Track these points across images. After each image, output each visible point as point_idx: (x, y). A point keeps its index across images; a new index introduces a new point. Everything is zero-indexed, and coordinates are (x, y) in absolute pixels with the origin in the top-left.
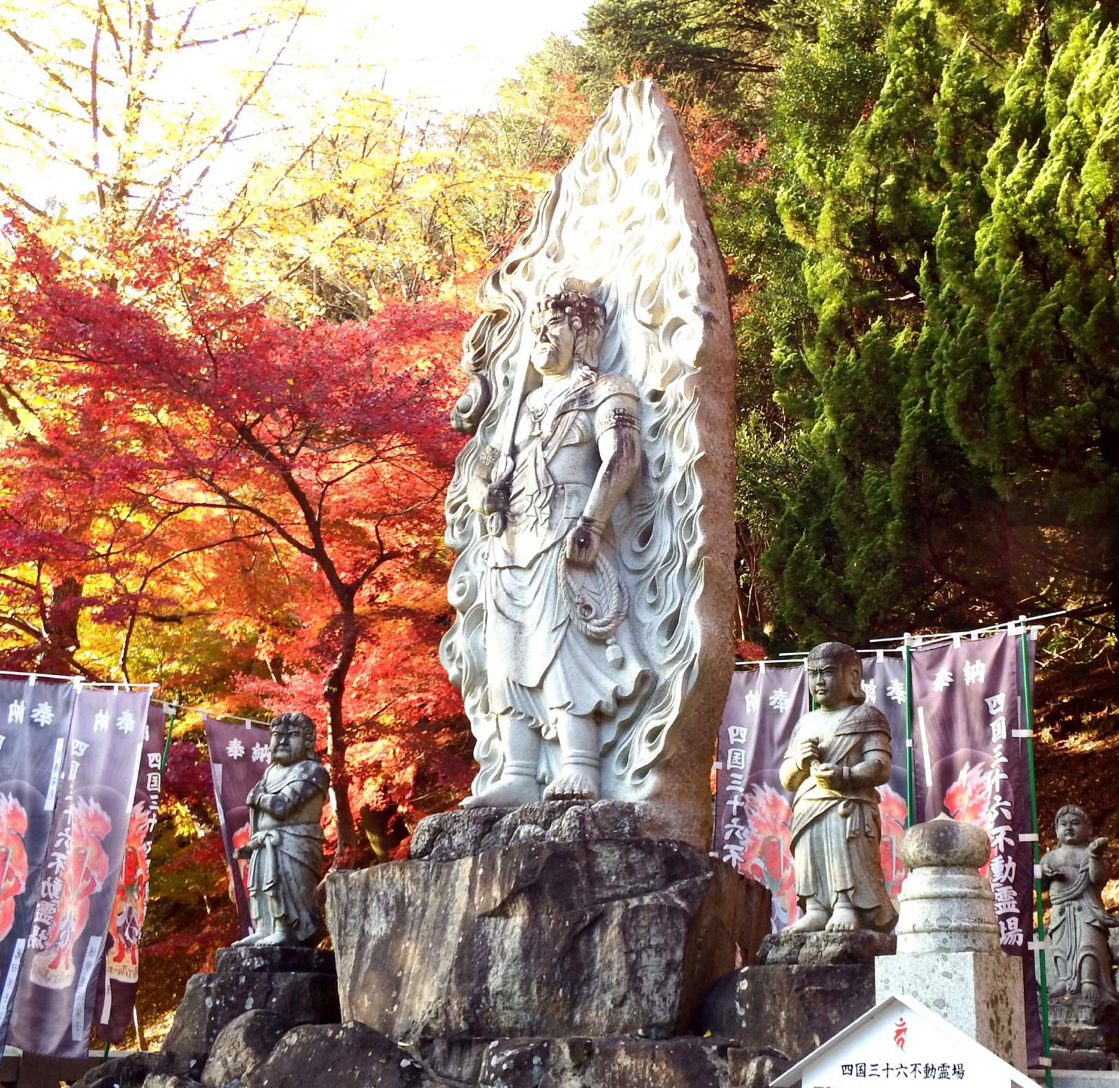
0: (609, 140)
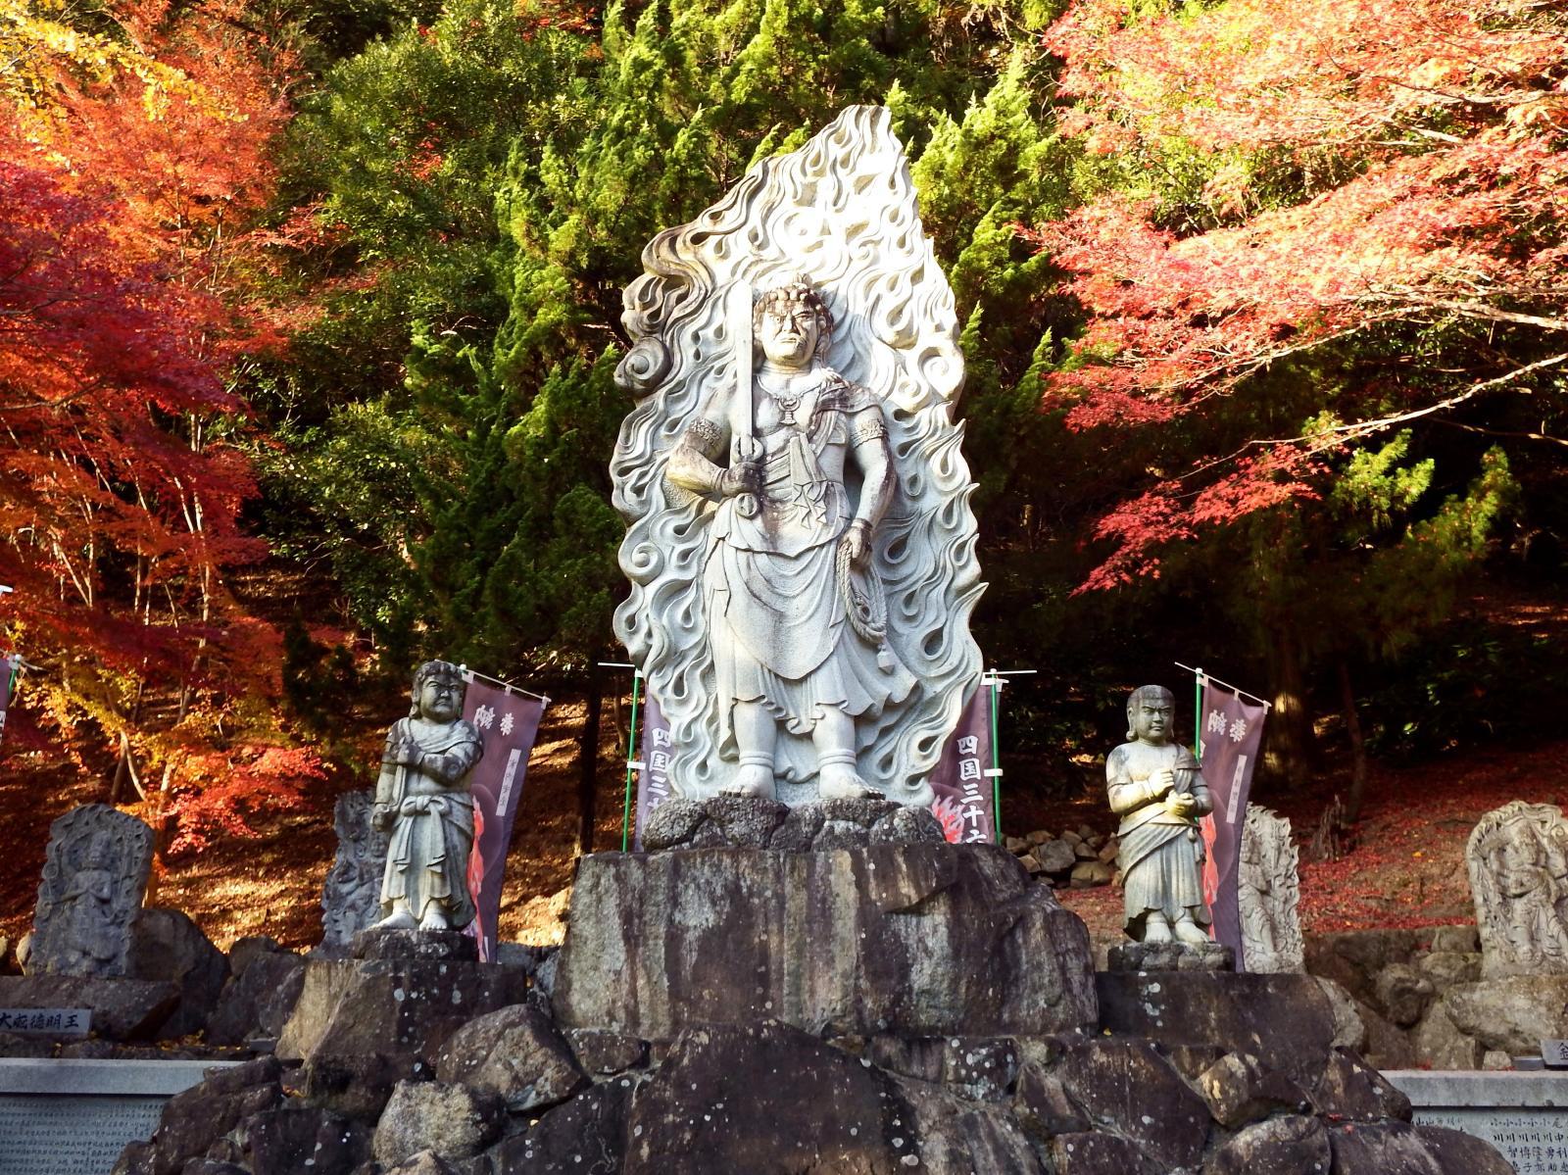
0: (837, 151)
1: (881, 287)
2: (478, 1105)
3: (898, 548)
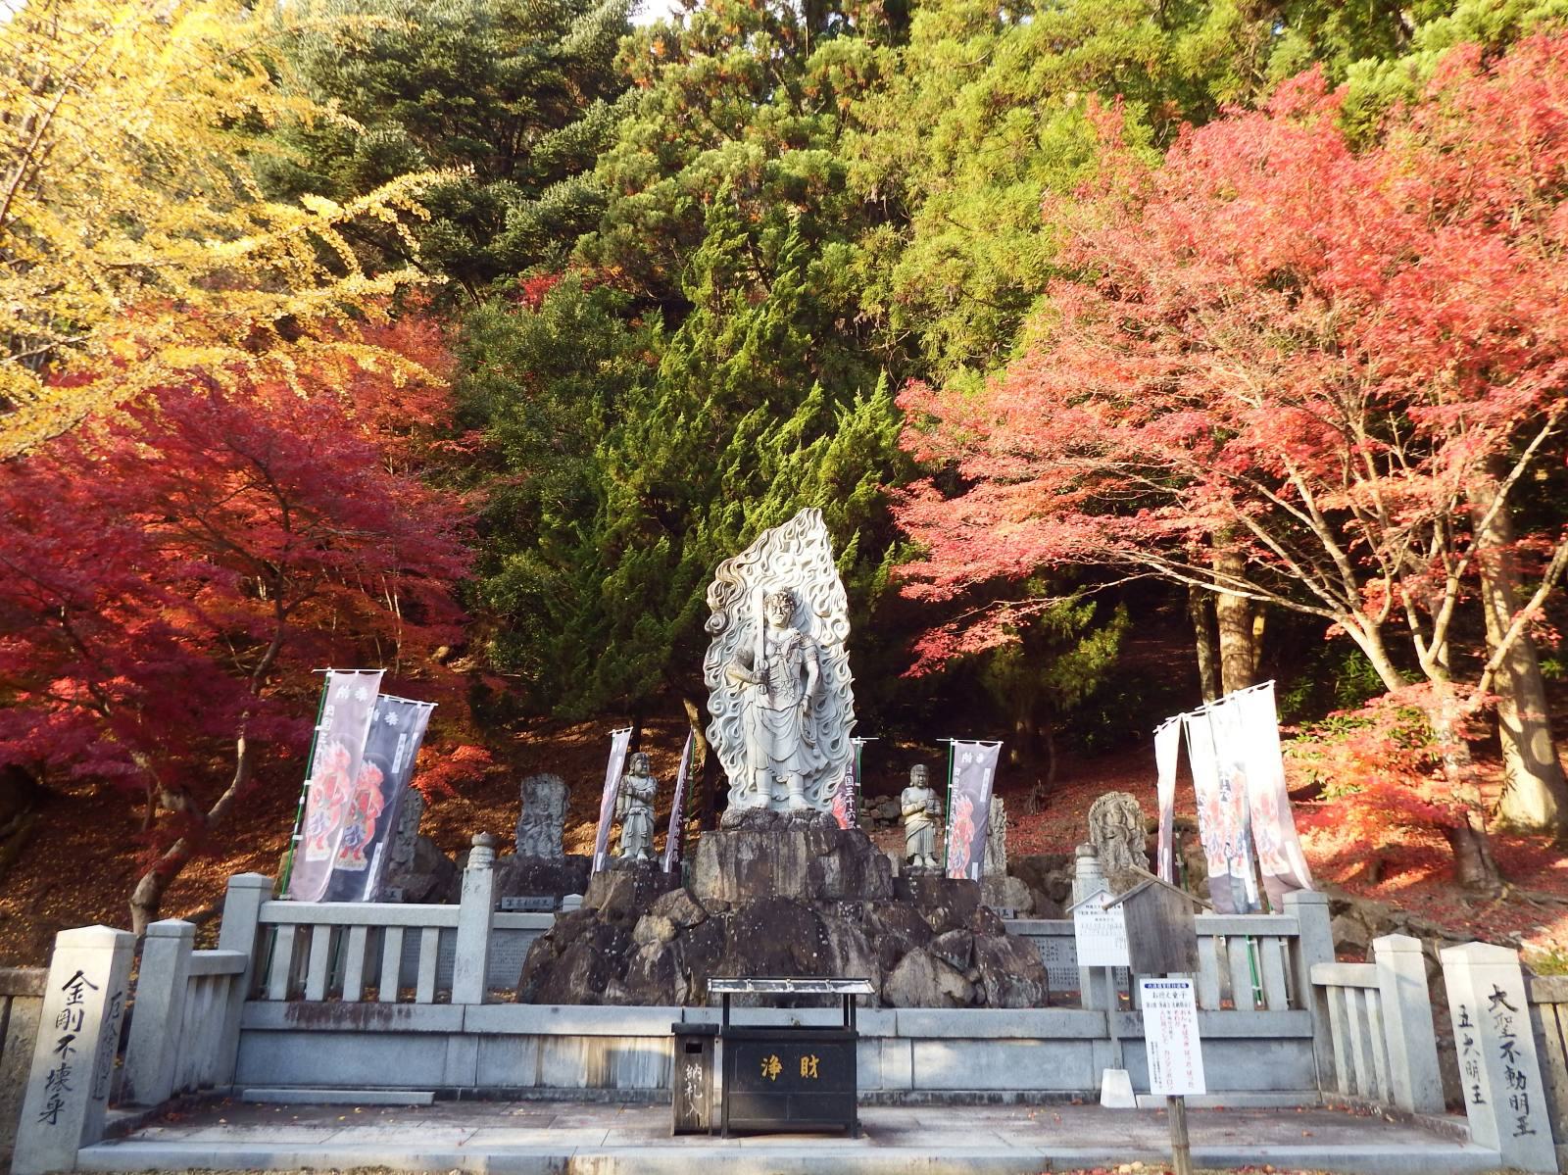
1: (817, 590)
2: (673, 924)
3: (822, 704)
